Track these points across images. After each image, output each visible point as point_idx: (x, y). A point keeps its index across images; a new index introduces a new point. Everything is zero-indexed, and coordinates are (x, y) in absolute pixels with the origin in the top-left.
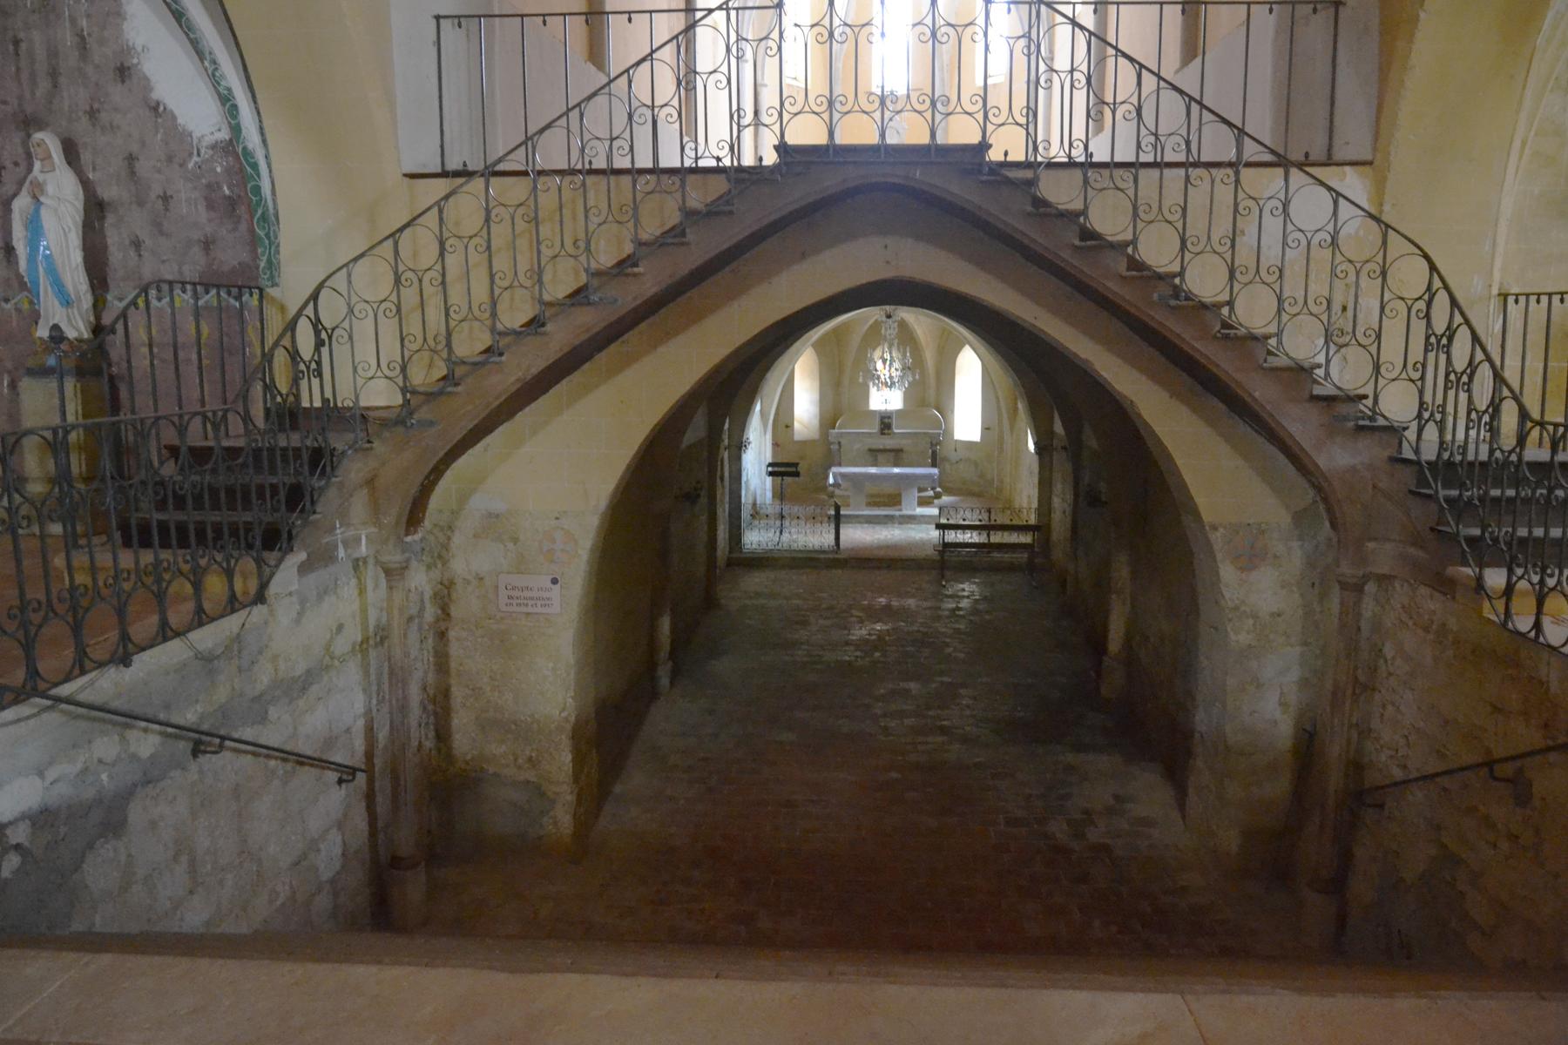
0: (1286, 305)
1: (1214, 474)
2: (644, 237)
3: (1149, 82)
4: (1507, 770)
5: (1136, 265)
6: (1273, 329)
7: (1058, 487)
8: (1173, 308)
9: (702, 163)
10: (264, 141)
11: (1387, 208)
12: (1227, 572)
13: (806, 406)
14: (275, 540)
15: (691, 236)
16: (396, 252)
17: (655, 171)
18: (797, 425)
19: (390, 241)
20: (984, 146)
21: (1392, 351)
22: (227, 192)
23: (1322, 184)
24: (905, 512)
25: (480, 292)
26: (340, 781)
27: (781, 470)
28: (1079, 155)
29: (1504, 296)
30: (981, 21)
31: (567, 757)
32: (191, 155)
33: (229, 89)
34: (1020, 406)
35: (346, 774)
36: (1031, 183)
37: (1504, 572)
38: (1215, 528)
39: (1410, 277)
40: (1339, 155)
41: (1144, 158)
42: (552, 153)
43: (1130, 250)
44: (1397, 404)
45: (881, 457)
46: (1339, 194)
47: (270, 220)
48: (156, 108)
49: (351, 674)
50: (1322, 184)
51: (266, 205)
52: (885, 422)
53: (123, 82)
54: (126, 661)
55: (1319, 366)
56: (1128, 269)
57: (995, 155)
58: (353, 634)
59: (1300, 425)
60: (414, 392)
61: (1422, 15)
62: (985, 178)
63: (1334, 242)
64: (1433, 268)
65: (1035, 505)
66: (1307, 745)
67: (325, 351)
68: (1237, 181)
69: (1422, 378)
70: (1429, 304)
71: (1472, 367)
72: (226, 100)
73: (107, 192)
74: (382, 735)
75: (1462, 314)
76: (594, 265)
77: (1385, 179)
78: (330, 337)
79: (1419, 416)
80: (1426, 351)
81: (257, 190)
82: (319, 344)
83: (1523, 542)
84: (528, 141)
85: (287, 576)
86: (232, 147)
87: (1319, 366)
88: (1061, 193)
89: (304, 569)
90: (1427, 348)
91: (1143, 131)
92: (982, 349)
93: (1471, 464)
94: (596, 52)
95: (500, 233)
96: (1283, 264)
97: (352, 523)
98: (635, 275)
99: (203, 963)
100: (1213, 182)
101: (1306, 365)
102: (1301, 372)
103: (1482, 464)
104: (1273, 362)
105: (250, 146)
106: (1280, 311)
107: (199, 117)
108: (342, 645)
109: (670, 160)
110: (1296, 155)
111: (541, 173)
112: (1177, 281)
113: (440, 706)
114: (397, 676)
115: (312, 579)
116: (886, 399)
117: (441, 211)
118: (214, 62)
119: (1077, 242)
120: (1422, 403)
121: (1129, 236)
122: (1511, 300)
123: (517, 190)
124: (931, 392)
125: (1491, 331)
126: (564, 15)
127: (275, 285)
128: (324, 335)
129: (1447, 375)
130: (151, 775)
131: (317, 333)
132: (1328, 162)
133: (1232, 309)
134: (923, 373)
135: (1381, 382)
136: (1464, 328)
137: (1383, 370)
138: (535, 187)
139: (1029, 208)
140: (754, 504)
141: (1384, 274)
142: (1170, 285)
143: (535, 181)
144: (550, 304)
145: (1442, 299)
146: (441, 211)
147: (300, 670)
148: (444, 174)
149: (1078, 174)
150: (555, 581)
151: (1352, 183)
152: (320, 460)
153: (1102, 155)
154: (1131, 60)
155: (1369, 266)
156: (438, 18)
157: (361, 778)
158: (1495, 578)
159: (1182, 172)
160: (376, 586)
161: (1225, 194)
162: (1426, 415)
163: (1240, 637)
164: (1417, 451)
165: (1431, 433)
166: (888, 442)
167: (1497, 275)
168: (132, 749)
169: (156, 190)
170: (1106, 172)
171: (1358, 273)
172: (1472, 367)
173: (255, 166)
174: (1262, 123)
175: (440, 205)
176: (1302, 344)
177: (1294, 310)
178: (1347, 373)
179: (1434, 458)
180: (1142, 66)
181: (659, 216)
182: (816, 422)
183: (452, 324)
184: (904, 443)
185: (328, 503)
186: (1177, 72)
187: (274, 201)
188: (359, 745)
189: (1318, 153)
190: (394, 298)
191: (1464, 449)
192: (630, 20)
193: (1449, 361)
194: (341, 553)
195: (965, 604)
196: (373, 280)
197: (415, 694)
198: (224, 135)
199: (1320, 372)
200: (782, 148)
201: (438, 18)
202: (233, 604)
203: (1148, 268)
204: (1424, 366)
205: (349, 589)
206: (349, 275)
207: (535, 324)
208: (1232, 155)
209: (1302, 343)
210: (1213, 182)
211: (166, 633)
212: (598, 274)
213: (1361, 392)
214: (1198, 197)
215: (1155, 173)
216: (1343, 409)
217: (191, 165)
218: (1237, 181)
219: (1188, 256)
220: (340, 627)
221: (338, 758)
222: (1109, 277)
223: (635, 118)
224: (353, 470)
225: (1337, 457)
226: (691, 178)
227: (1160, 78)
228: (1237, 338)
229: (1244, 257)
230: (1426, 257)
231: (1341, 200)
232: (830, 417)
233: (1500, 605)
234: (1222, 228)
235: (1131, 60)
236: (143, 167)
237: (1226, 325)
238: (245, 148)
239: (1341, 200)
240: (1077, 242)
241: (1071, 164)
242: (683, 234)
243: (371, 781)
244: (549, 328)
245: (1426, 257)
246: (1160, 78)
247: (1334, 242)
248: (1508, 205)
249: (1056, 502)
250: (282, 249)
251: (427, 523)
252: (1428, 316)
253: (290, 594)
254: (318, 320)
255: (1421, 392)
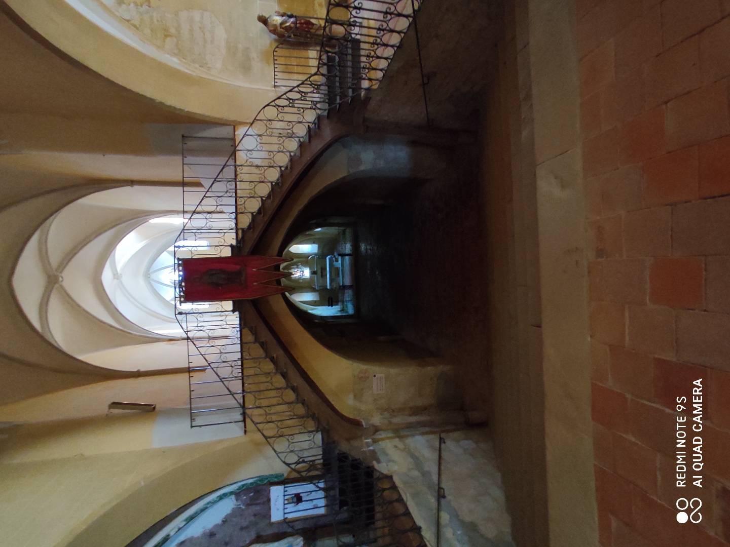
0: (280, 150)
1: (336, 170)
2: (264, 355)
3: (208, 194)
4: (426, 81)
5: (269, 196)
6: (288, 154)
7: (332, 221)
8: (282, 184)
9: (239, 336)
10: (235, 483)
11: (248, 121)
12: (362, 168)
13: (308, 297)
14: (370, 472)
15: (263, 340)
16: (272, 437)
17: (242, 352)
18: (315, 299)
19: (279, 454)
20: (231, 246)
21: (294, 118)
22: (252, 494)
23: (240, 142)
24: (340, 266)
25: (273, 393)
26: (444, 443)
27: (331, 302)
28: (233, 216)
29: (275, 86)
30: (190, 248)
31: (429, 368)
32: (240, 508)
33: (218, 497)
34: (308, 233)
35: (442, 441)
36: (243, 230)
37: (363, 81)
38: (349, 172)
39: (271, 112)
40: (231, 136)
41: (234, 195)
42: (237, 386)
43: (264, 199)
44: (311, 116)
45: (324, 274)
46: (245, 134)
47: (262, 478)
48: (224, 522)
49: (409, 441)
50: (240, 142)
51: (257, 480)
52: (313, 273)
53: (215, 534)
54: (420, 528)
55: (299, 140)
56: (270, 198)
57: (234, 243)
58: (396, 441)
59: (318, 146)
60: (318, 428)
61: (186, 110)
62: (242, 245)
63: (260, 136)
64: (268, 105)
65: (337, 228)
66: (413, 143)
67: (306, 460)
68: (241, 166)
69: (303, 108)
70: (279, 106)
71: (299, 92)
72: (221, 498)
73: (253, 535)
74: (427, 429)
75: (282, 95)
76: (274, 371)
77: (239, 122)
78: (302, 458)
79: (314, 109)
80: (294, 107)
81: (251, 484)
82: (304, 462)
83: (353, 74)
84: (232, 394)
85: (382, 468)
86: (237, 494)
87: (299, 140)
88: (245, 221)
89: (379, 462)
90: (293, 107)
91: (226, 195)
92: (290, 245)
93: (328, 92)
94: (202, 370)
95: (264, 403)
96: (264, 154)
97: (363, 446)
98: (277, 357)
99: (87, 197)
100: (241, 173)
101: (299, 144)
102: (301, 145)
103: (329, 88)
104: (298, 154)
105: (237, 488)
106: (282, 152)
107: (227, 506)
108: (401, 446)
109: (238, 348)
110: (233, 148)
111: (243, 391)
112: (274, 184)
113: (416, 411)
114: (409, 426)
115: (382, 458)
116: (306, 273)
117: (258, 423)
118: (208, 503)
119: (262, 215)
120: (311, 108)
121: (260, 199)
122: (276, 84)
123: (250, 398)
124: (304, 260)
125: (285, 89)
126: (190, 384)
127: (283, 475)
128: (301, 460)
129: (302, 100)
130: (455, 515)
131: (300, 463)
132: (234, 139)
133: (282, 167)
134: (299, 262)
135: (304, 121)
136: (287, 94)
137: (300, 121)
138: (249, 392)
139: (252, 230)
140: (340, 311)
141: (270, 120)
142: (275, 186)
143: (247, 392)
144: (287, 385)
145: (279, 102)
146: (258, 423)
147: (410, 460)
148: (244, 421)
149: (240, 216)
150: (375, 376)
151: (240, 131)
152: (343, 457)
153: (233, 209)
154: (203, 199)
155: (267, 125)
156: (192, 427)
157: (443, 435)
158: (365, 84)
159: (238, 183)
160: (380, 435)
161: (245, 169)
162: (314, 107)
163: (381, 164)
164: (325, 110)
165: (318, 106)
166: (319, 272)
167: (269, 88)
168: (448, 522)
169: (253, 518)
170: (238, 207)
171: (270, 128)
172: (299, 92)
173: (243, 485)
174: (222, 160)
175: (256, 424)
176: (293, 145)
177: (282, 147)
178: (301, 131)
179: (327, 105)
180: (204, 196)
181: (258, 351)
182: (313, 293)
183: (273, 388)
184: (319, 267)
185: (355, 454)
186: (205, 188)
187: (255, 478)
188: (431, 436)
189: (231, 143)
190: (287, 437)
191: (325, 94)
192: (191, 362)
193: (297, 100)
194: (371, 448)
195: (368, 247)
196: (282, 445)
197: (413, 419)
198: (233, 497)
199: (302, 140)
200: (233, 311)
201: (192, 427)
202: (394, 487)
203: (270, 193)
204: (299, 108)
205: (382, 444)
206: (280, 453)
207: (294, 389)
208: (233, 168)
209: (293, 145)
210: (241, 173)
211: (407, 514)
212: (277, 370)
213: (307, 127)
214: (246, 177)
215: (238, 191)
216: (312, 133)
217: (244, 507)
218: (241, 166)
219: (266, 181)
220: (396, 447)
221: (437, 444)
222: (272, 206)
223: (224, 360)
224: (344, 447)
225: (328, 134)
226: (244, 341)
227: (199, 205)
228: (291, 165)
229: (266, 163)
230: (264, 107)
231: (257, 118)
232: (313, 290)
233: (374, 82)
234: (254, 170)
235: (203, 199)
236: (245, 524)
237: (286, 168)
238: (237, 489)
239: (257, 118)
240: (262, 215)
241: (236, 218)
242: (263, 342)
243: (443, 431)
244: (295, 385)
245: (264, 107)
246: (199, 205)
247: (260, 136)
248: (247, 85)
249: (336, 221)
250: (271, 473)
251: (358, 418)
252: (283, 107)
253: (387, 465)
254: (296, 463)
255: (307, 109)
